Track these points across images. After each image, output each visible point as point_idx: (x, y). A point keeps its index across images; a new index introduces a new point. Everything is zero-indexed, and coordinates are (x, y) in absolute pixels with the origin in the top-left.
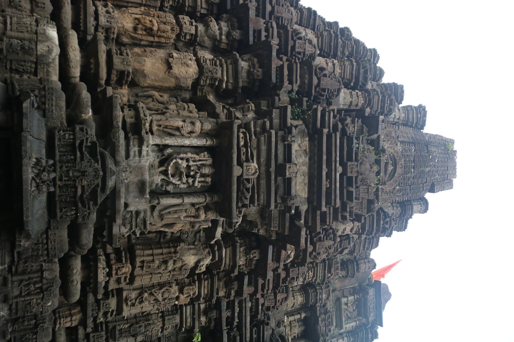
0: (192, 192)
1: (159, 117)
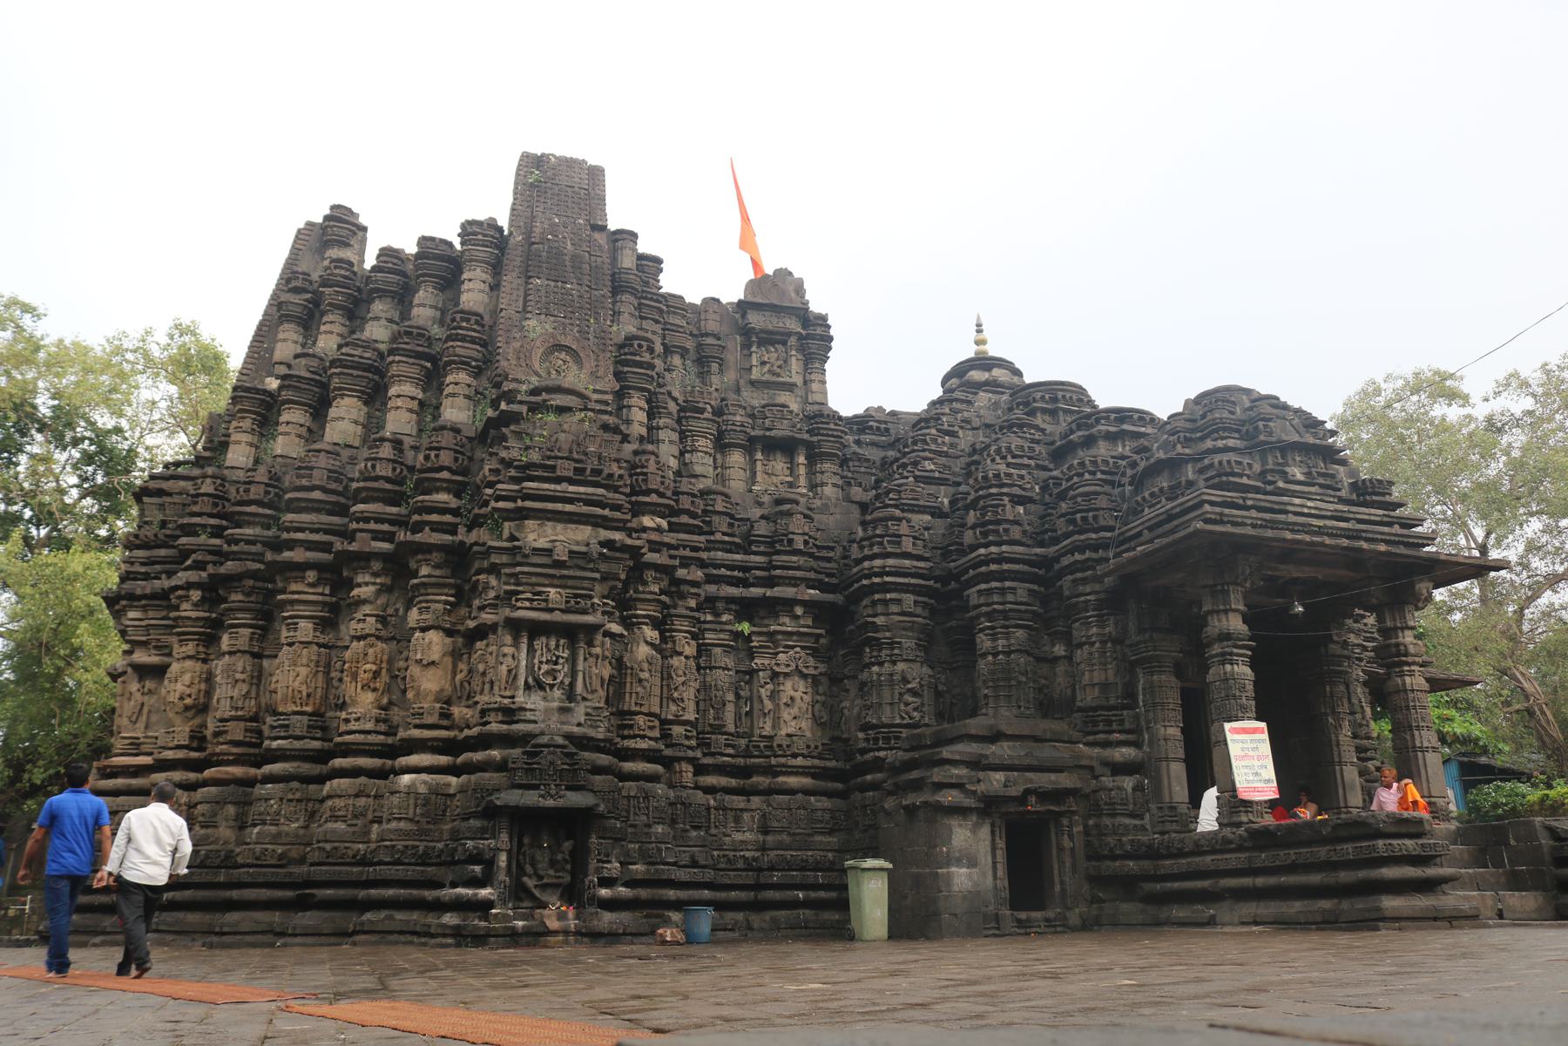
1: (496, 688)
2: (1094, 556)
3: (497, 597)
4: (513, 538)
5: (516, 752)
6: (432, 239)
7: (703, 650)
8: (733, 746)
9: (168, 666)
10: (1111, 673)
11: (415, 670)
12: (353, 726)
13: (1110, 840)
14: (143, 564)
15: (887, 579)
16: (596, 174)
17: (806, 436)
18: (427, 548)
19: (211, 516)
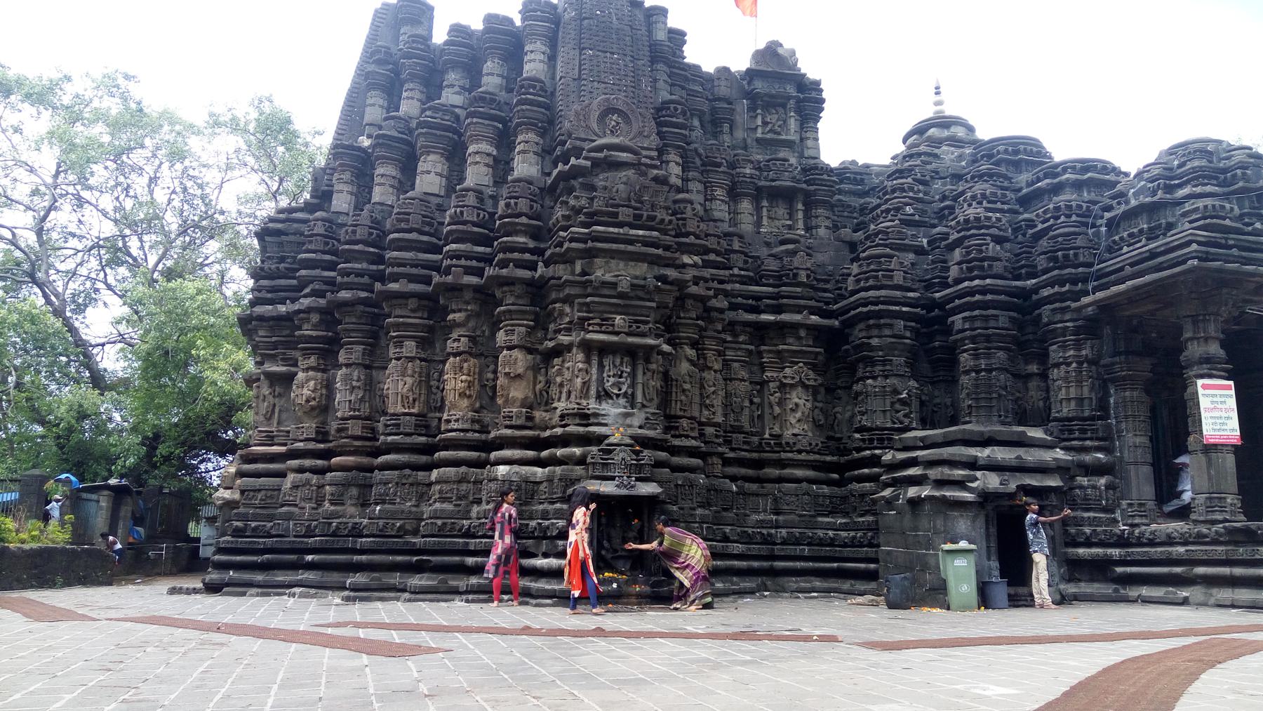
0: (633, 375)
1: (573, 396)
3: (570, 322)
4: (584, 273)
5: (594, 449)
7: (726, 364)
10: (1086, 390)
13: (1087, 530)
14: (268, 292)
17: (804, 186)
18: (509, 282)
19: (324, 252)
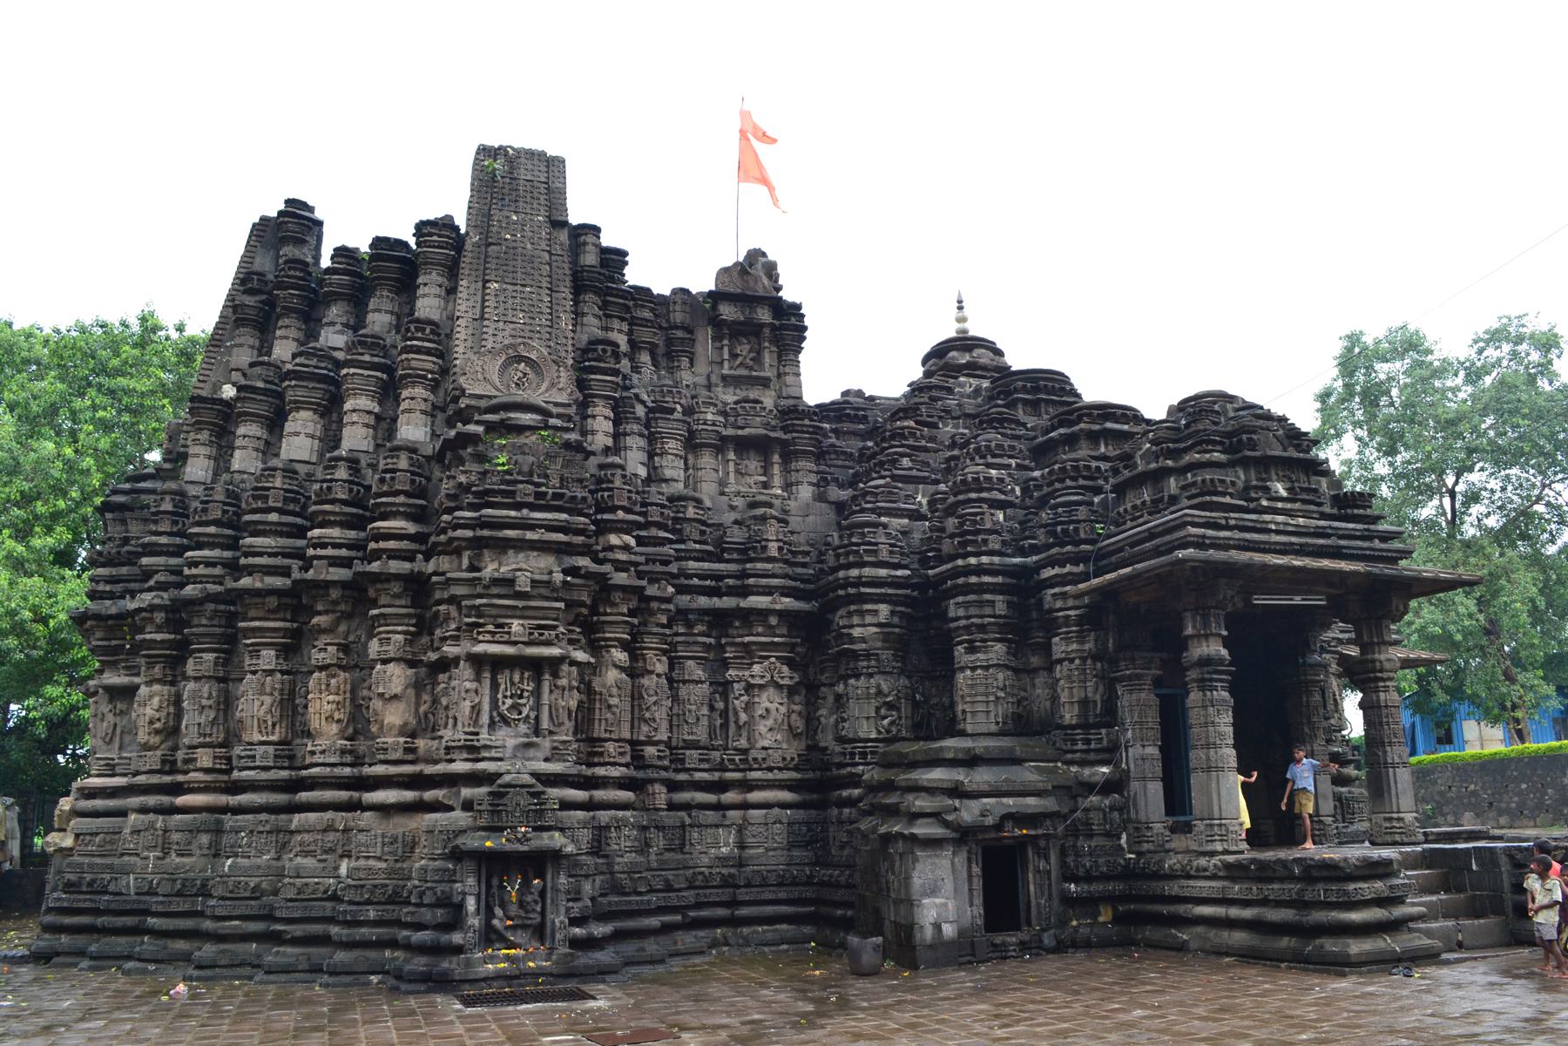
0: (537, 694)
2: (1075, 569)
3: (458, 629)
6: (386, 239)
8: (707, 761)
9: (137, 687)
11: (376, 704)
12: (318, 759)
14: (107, 582)
15: (863, 590)
16: (554, 166)
17: (779, 434)
